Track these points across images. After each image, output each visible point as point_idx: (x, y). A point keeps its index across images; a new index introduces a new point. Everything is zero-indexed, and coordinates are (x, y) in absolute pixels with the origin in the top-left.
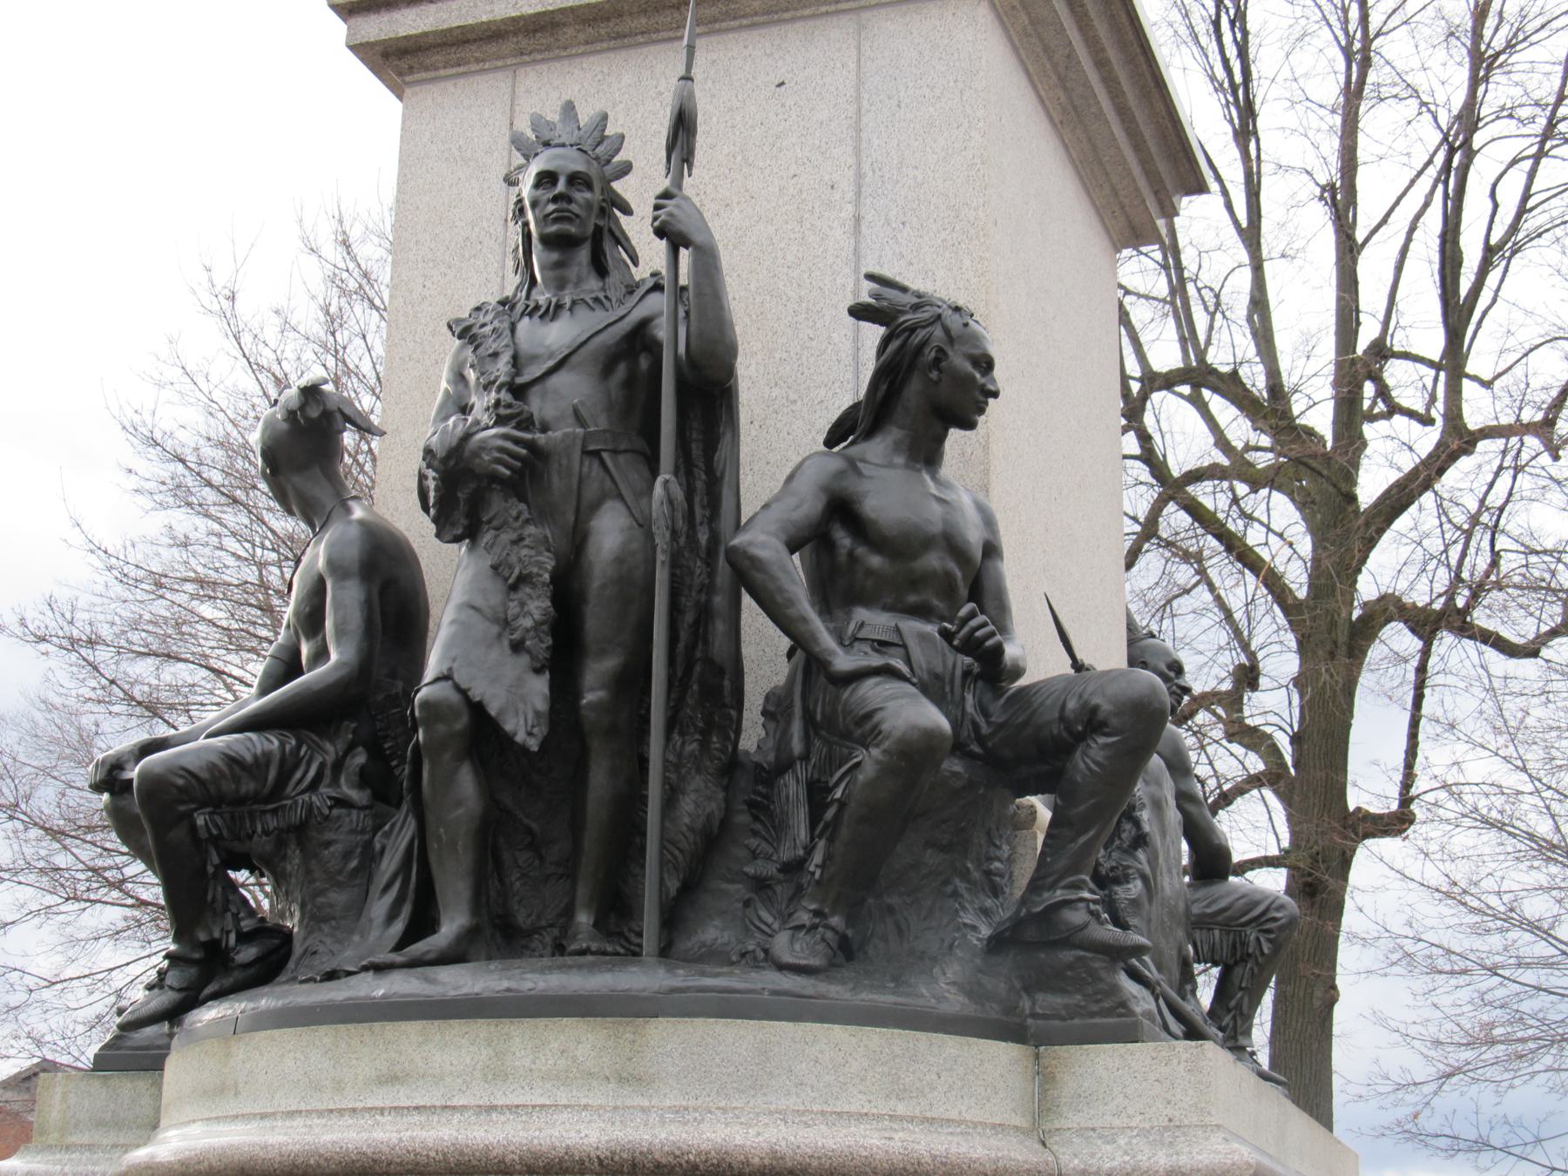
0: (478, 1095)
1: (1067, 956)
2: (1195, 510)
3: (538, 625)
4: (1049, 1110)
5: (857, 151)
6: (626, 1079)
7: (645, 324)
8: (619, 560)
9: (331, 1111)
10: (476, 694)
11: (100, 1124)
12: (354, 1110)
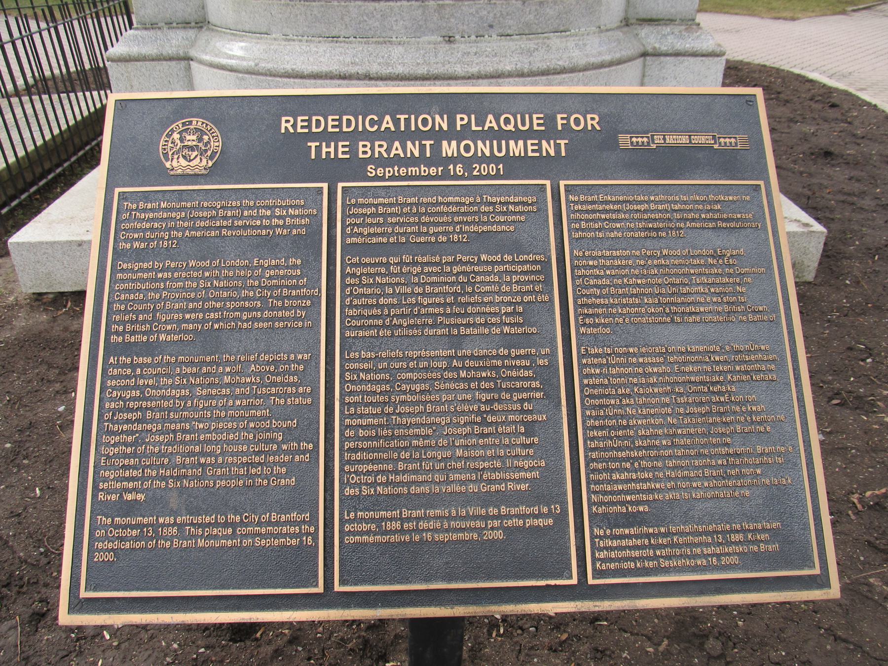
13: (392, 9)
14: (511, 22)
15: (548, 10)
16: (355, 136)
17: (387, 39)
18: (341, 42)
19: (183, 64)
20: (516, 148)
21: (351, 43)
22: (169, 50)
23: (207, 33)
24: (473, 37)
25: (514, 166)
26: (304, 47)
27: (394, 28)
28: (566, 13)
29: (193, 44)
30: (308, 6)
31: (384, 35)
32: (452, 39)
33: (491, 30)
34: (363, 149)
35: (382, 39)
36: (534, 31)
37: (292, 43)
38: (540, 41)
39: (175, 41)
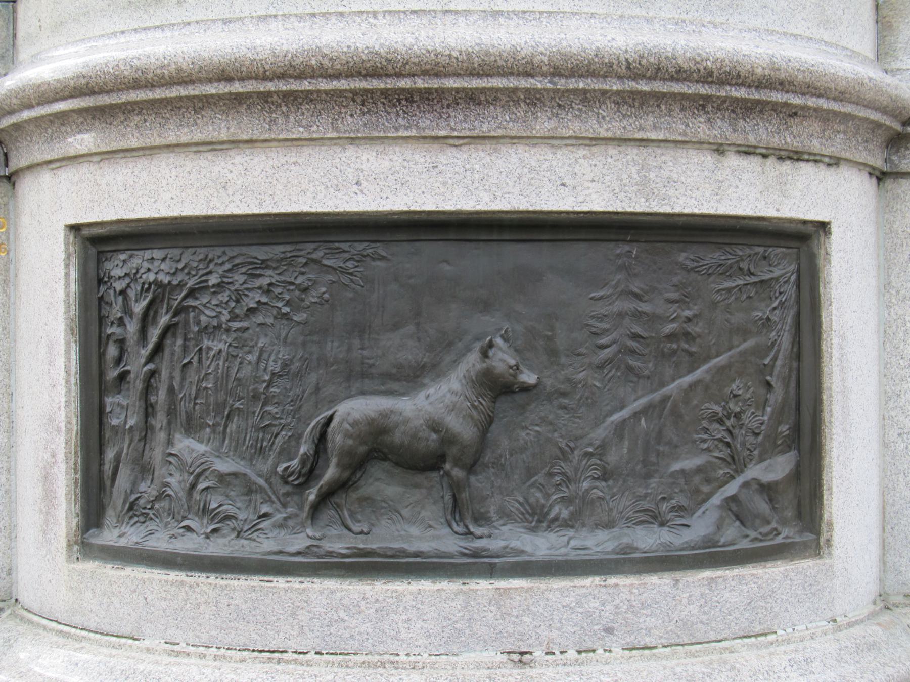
4: (886, 53)
9: (314, 15)
12: (341, 14)
13: (399, 597)
14: (651, 622)
15: (727, 595)
17: (386, 657)
18: (288, 662)
21: (309, 664)
23: (10, 624)
24: (572, 654)
26: (208, 671)
27: (404, 635)
28: (764, 598)
30: (223, 588)
31: (380, 649)
32: (527, 657)
33: (609, 641)
35: (376, 658)
36: (700, 637)
37: (185, 660)
38: (715, 657)
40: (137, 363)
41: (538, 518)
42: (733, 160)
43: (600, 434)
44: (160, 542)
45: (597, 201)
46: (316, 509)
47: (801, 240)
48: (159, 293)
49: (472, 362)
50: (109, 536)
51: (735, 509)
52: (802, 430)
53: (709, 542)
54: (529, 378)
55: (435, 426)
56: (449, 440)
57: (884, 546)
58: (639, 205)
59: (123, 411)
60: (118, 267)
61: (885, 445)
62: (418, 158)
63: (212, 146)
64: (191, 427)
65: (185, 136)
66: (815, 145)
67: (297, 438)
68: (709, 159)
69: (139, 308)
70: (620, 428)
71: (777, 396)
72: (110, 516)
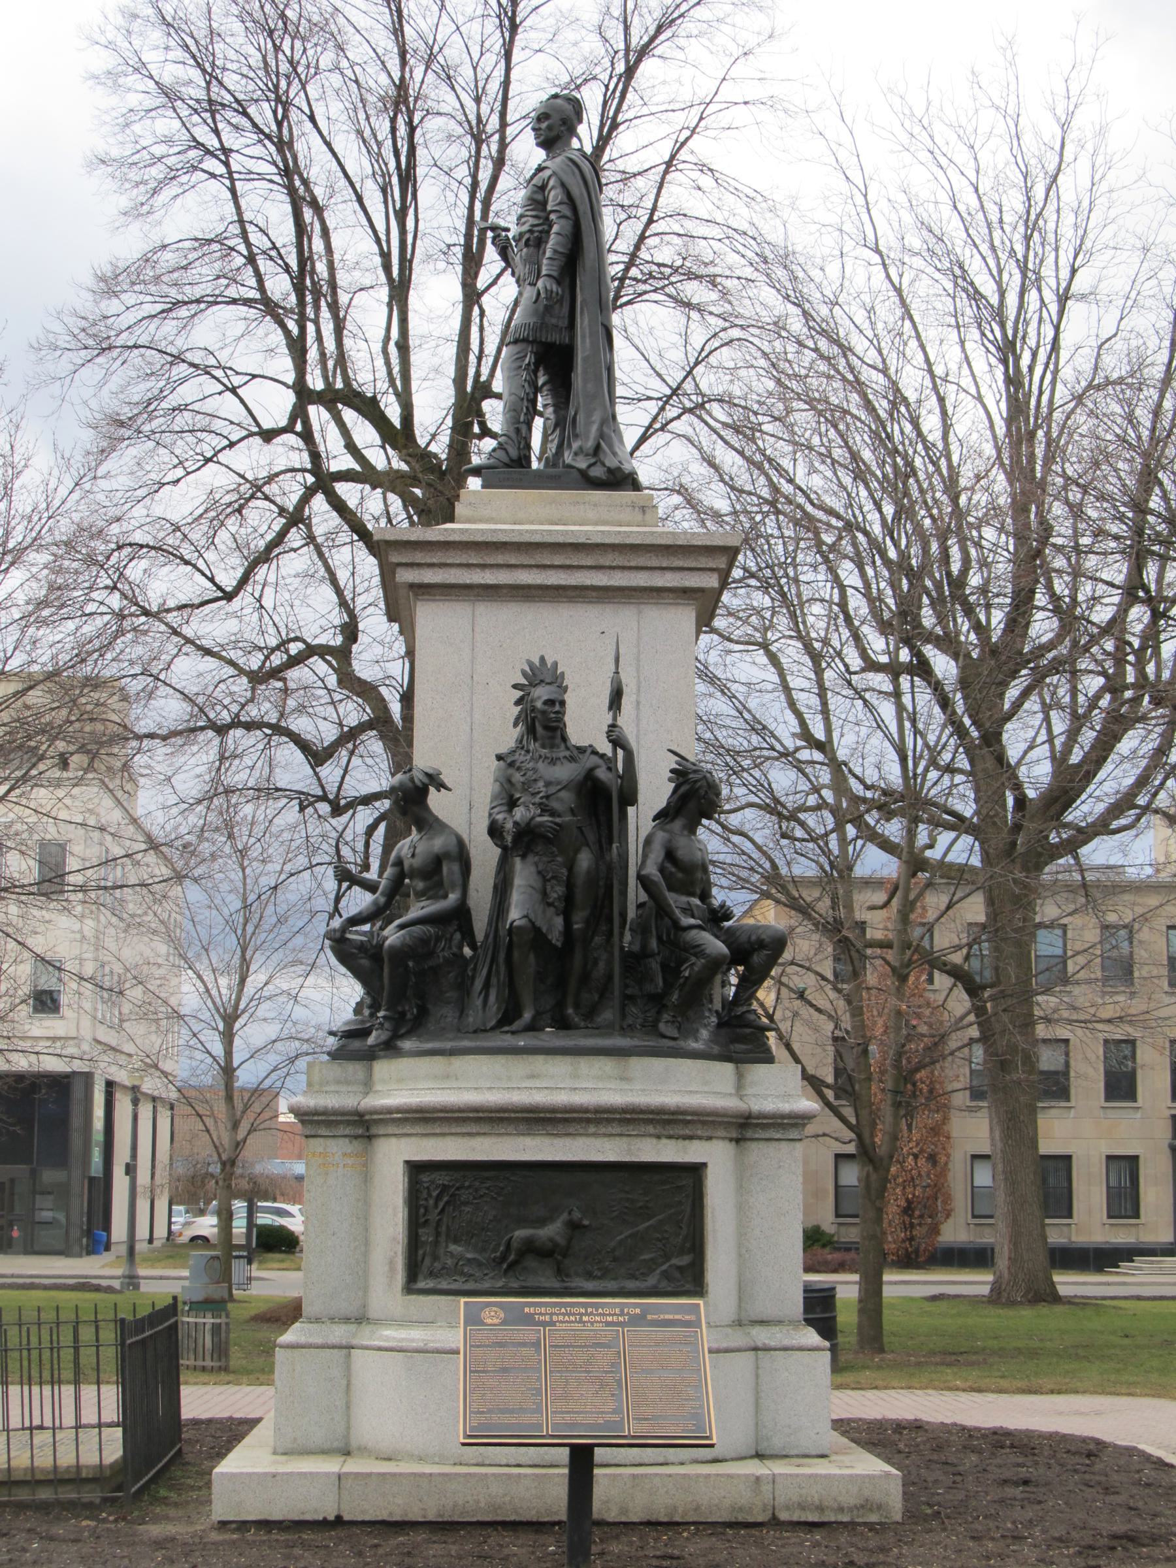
0: (568, 1083)
1: (748, 1031)
2: (339, 506)
3: (559, 898)
5: (638, 671)
6: (622, 1079)
7: (592, 770)
8: (588, 872)
10: (538, 924)
11: (338, 1082)
16: (551, 1314)
19: (344, 1351)
20: (610, 1319)
22: (333, 1339)
25: (608, 1324)
29: (354, 1335)
34: (555, 1318)
39: (339, 1333)
40: (433, 1216)
41: (589, 1276)
42: (664, 1141)
43: (613, 1244)
44: (444, 1285)
45: (612, 1157)
46: (506, 1271)
47: (696, 1171)
48: (445, 1188)
49: (565, 1216)
50: (421, 1285)
51: (666, 1275)
52: (695, 1245)
53: (655, 1287)
54: (586, 1222)
55: (551, 1240)
56: (556, 1245)
57: (740, 1299)
58: (627, 1159)
59: (426, 1235)
60: (425, 1178)
61: (740, 1255)
62: (547, 1141)
63: (470, 1134)
64: (456, 1241)
65: (459, 1130)
66: (699, 1133)
67: (499, 1245)
68: (654, 1141)
69: (435, 1194)
70: (621, 1242)
71: (684, 1232)
72: (420, 1277)
